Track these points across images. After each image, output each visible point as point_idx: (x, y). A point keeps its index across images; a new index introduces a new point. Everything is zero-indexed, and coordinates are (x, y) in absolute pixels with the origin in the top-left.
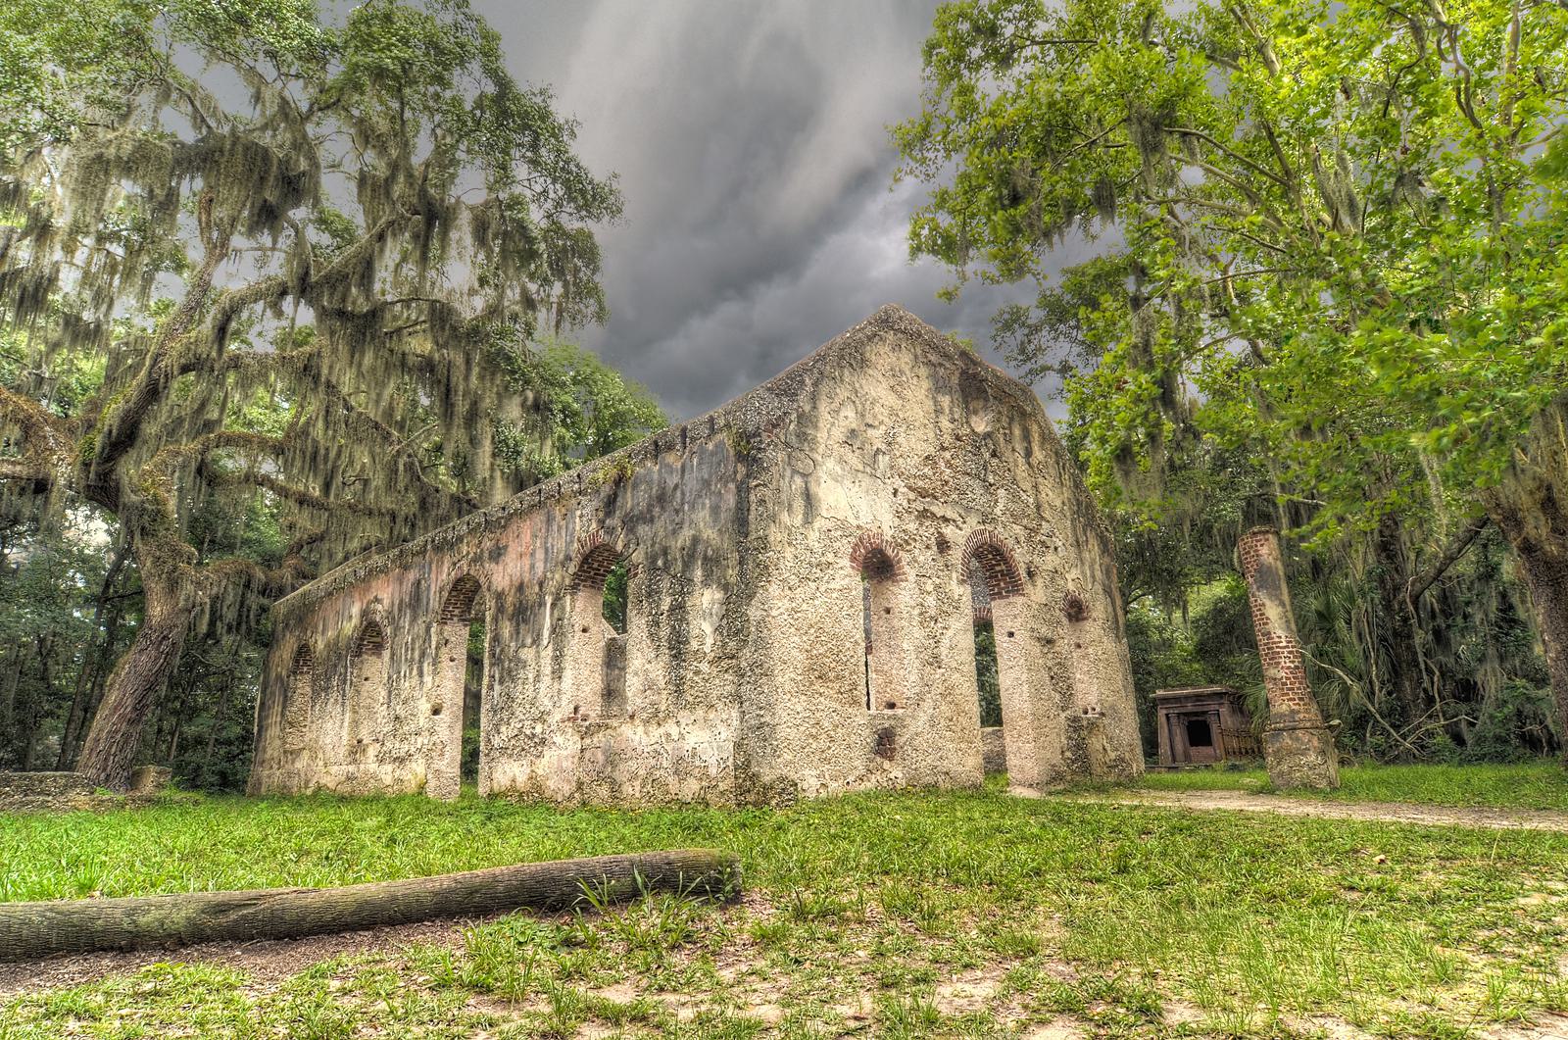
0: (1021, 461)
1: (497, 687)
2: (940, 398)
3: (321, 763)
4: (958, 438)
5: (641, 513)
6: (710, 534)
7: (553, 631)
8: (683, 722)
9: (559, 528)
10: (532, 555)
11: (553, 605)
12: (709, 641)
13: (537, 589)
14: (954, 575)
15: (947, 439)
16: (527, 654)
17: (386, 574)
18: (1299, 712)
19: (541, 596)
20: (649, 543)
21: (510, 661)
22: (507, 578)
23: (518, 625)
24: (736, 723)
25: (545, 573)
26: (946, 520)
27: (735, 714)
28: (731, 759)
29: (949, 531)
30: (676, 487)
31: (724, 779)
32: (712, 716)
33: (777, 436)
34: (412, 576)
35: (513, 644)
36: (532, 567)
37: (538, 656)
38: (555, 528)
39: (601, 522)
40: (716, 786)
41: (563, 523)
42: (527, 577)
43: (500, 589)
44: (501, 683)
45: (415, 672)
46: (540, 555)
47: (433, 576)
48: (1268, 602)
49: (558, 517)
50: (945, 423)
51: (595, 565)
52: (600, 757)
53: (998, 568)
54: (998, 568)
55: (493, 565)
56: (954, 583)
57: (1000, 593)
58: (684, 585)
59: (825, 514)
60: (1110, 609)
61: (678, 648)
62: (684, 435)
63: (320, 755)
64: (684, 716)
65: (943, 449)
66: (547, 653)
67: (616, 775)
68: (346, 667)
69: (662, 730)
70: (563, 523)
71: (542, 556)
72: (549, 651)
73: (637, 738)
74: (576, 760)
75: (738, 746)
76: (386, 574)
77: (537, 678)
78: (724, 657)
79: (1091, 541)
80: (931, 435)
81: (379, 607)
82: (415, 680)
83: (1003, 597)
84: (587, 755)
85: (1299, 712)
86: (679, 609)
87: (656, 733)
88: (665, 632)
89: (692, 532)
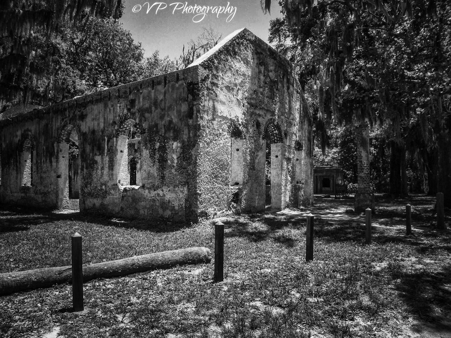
0: (286, 91)
1: (85, 170)
2: (261, 67)
3: (9, 192)
4: (266, 83)
5: (147, 108)
6: (175, 120)
7: (109, 150)
8: (165, 190)
9: (110, 110)
10: (99, 119)
11: (108, 141)
12: (176, 161)
13: (101, 133)
14: (261, 136)
15: (262, 84)
16: (98, 158)
17: (32, 120)
18: (367, 188)
19: (103, 136)
20: (150, 120)
21: (90, 161)
22: (87, 128)
23: (93, 147)
24: (186, 192)
25: (104, 127)
26: (259, 115)
27: (186, 189)
28: (184, 204)
29: (260, 119)
30: (161, 100)
31: (181, 211)
32: (176, 189)
33: (204, 84)
34: (44, 122)
35: (91, 154)
36: (99, 124)
37: (102, 159)
38: (108, 110)
39: (129, 110)
40: (178, 213)
41: (112, 108)
42: (96, 128)
43: (84, 132)
44: (87, 168)
45: (48, 161)
46: (102, 120)
47: (54, 123)
48: (363, 151)
49: (110, 106)
50: (262, 77)
51: (126, 126)
52: (130, 199)
53: (275, 132)
54: (275, 132)
55: (81, 122)
56: (261, 138)
57: (274, 141)
58: (164, 140)
59: (219, 115)
60: (309, 146)
61: (163, 161)
62: (165, 80)
63: (9, 189)
64: (165, 189)
65: (260, 87)
66: (107, 159)
67: (137, 206)
68: (17, 156)
69: (156, 192)
70: (112, 108)
71: (103, 121)
72: (107, 159)
73: (146, 194)
74: (120, 200)
75: (186, 200)
76: (32, 120)
77: (102, 168)
78: (180, 167)
79: (306, 122)
80: (257, 82)
81: (30, 133)
82: (48, 164)
83: (275, 143)
84: (125, 198)
85: (367, 188)
86: (163, 149)
87: (153, 193)
88: (157, 156)
89: (169, 119)
